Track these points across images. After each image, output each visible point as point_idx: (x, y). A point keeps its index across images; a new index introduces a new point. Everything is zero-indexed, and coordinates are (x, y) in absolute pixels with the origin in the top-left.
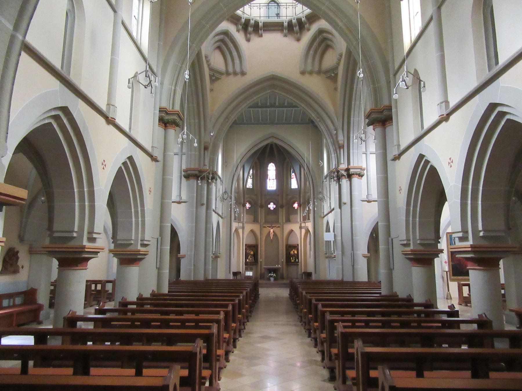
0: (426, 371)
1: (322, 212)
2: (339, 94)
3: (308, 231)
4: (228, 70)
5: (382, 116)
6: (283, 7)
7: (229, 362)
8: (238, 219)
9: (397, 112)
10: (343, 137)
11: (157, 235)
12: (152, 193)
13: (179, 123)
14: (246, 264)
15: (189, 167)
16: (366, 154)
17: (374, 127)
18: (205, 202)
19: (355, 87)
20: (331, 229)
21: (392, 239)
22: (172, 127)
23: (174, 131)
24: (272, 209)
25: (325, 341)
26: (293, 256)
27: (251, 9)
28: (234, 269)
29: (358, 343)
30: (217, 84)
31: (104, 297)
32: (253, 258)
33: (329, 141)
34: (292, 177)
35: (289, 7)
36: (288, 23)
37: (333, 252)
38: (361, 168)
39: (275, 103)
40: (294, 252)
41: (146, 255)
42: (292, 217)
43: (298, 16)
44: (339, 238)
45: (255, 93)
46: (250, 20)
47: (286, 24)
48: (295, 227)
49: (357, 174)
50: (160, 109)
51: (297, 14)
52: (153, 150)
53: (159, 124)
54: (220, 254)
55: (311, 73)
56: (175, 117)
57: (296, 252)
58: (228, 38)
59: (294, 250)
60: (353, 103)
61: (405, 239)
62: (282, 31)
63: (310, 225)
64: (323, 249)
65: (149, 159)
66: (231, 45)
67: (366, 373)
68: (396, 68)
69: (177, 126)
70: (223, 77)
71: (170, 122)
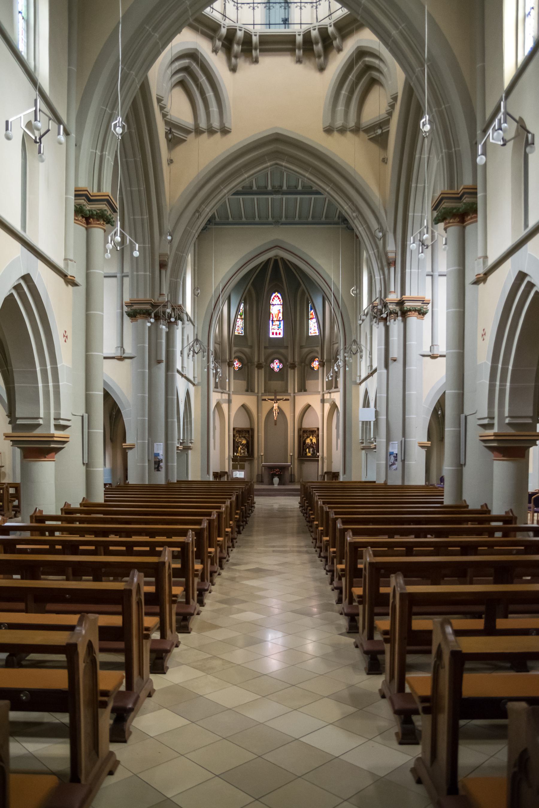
0: (499, 618)
1: (358, 375)
2: (390, 168)
3: (334, 406)
4: (198, 125)
5: (461, 206)
6: (296, 5)
7: (204, 606)
8: (220, 386)
9: (485, 197)
10: (394, 245)
11: (82, 411)
12: (69, 340)
13: (110, 218)
14: (235, 459)
15: (135, 298)
16: (432, 276)
17: (446, 224)
18: (164, 358)
19: (417, 156)
20: (372, 404)
21: (466, 417)
22: (99, 224)
23: (103, 231)
24: (276, 369)
25: (344, 575)
26: (311, 446)
27: (237, 9)
28: (215, 467)
29: (396, 578)
30: (180, 149)
31: (8, 510)
32: (246, 449)
33: (371, 252)
34: (310, 316)
35: (306, 5)
36: (304, 35)
37: (372, 439)
38: (423, 301)
39: (281, 187)
40: (311, 440)
41: (64, 442)
42: (310, 384)
43: (323, 23)
44: (383, 417)
45: (247, 166)
46: (236, 29)
47: (299, 39)
48: (314, 400)
49: (415, 310)
50: (75, 191)
51: (319, 20)
52: (67, 265)
53: (75, 219)
54: (191, 443)
55: (342, 131)
56: (104, 206)
57: (314, 440)
58: (197, 64)
59: (311, 437)
60: (413, 185)
61: (486, 416)
62: (292, 51)
63: (337, 397)
64: (357, 434)
65: (61, 280)
66: (203, 79)
67: (406, 622)
68: (488, 116)
69: (107, 223)
70: (191, 137)
71: (94, 215)
